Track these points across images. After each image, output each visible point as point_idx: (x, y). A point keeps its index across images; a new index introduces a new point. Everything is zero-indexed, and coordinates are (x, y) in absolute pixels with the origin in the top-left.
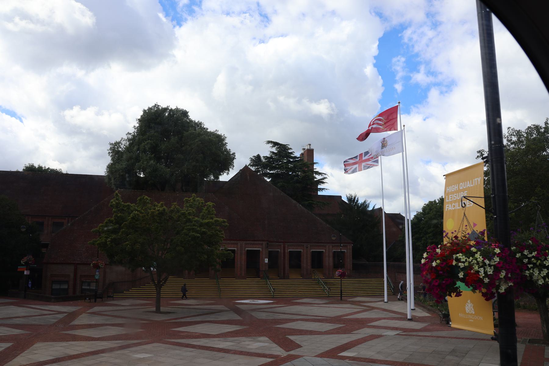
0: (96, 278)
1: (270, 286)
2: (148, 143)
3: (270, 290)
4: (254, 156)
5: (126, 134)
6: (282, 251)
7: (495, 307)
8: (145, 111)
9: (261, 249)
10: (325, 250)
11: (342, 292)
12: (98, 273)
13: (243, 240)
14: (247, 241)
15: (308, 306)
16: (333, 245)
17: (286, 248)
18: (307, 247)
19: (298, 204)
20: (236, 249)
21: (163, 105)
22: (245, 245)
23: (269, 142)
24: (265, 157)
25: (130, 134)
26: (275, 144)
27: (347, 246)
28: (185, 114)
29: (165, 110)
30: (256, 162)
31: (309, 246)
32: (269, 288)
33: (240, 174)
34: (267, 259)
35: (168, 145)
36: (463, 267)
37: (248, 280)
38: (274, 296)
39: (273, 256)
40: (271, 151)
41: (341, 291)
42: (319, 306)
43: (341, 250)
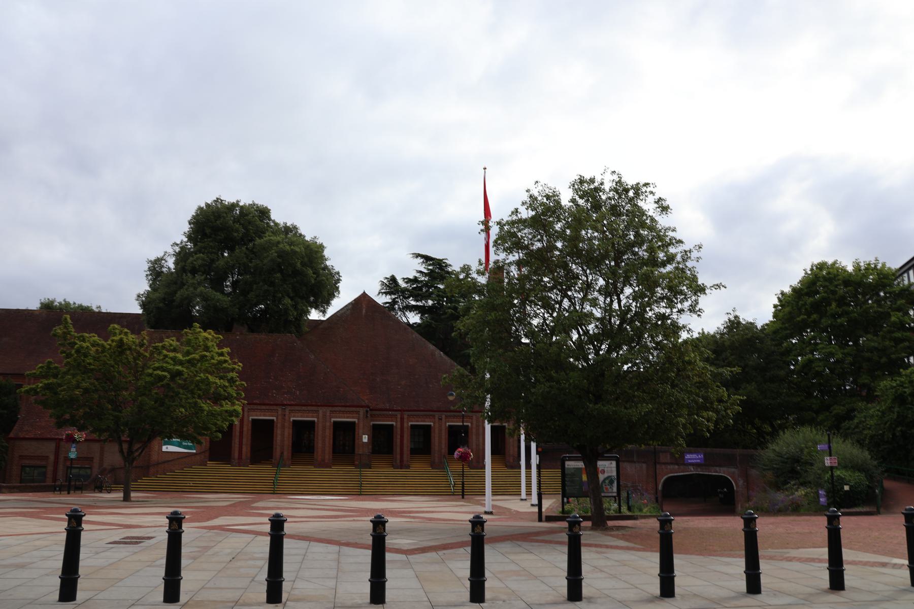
0: (71, 457)
1: (450, 479)
2: (197, 259)
3: (450, 484)
4: (386, 278)
5: (172, 246)
6: (399, 426)
9: (356, 420)
10: (472, 424)
11: (465, 491)
12: (75, 449)
13: (326, 406)
14: (333, 406)
17: (405, 420)
18: (441, 419)
19: (438, 351)
20: (432, 424)
21: (229, 199)
22: (330, 413)
23: (418, 256)
24: (406, 279)
25: (177, 245)
26: (427, 258)
27: (397, 415)
28: (264, 213)
29: (233, 206)
30: (391, 288)
31: (444, 416)
32: (449, 482)
33: (350, 306)
34: (367, 436)
35: (229, 260)
36: (539, 457)
37: (335, 468)
38: (362, 493)
39: (377, 431)
40: (417, 271)
41: (463, 482)
43: (463, 423)
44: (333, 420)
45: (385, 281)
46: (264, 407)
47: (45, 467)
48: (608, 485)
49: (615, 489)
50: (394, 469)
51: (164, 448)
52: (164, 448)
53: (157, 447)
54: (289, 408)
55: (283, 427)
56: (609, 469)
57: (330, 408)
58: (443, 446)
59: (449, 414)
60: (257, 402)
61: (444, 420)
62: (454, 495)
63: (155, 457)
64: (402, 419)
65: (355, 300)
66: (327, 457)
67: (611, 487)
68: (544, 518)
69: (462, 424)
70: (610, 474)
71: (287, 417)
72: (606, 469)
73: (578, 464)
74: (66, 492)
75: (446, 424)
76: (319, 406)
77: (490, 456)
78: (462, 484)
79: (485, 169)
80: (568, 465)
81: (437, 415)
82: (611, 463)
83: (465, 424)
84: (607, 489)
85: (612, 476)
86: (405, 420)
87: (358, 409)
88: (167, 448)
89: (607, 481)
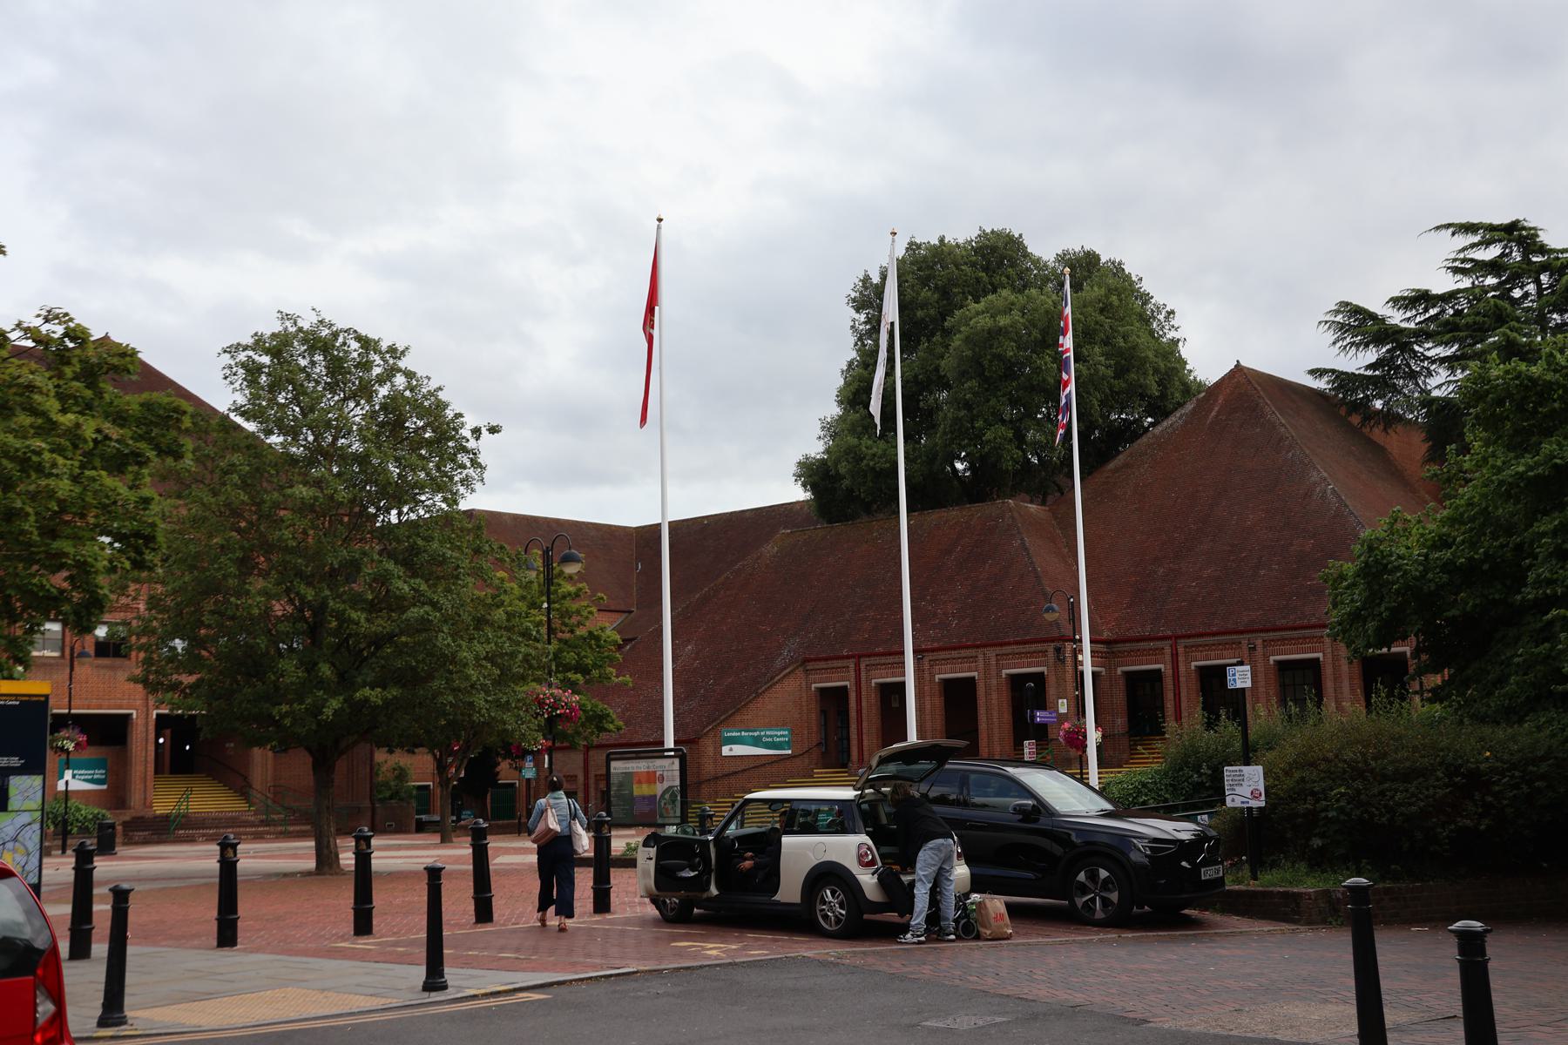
6: (1170, 672)
12: (532, 764)
14: (1001, 645)
18: (1254, 648)
26: (1391, 299)
31: (1259, 642)
34: (1065, 701)
43: (70, 709)
44: (1005, 672)
45: (1339, 318)
49: (678, 814)
51: (726, 751)
52: (726, 751)
56: (670, 773)
57: (998, 650)
60: (881, 649)
61: (1260, 649)
63: (709, 768)
64: (1175, 656)
69: (67, 711)
70: (670, 784)
71: (927, 675)
72: (665, 773)
73: (627, 765)
74: (60, 852)
75: (999, 675)
76: (978, 647)
79: (660, 220)
80: (615, 769)
81: (1244, 639)
82: (673, 763)
83: (73, 711)
86: (1181, 659)
87: (1159, 644)
88: (731, 750)
89: (667, 796)
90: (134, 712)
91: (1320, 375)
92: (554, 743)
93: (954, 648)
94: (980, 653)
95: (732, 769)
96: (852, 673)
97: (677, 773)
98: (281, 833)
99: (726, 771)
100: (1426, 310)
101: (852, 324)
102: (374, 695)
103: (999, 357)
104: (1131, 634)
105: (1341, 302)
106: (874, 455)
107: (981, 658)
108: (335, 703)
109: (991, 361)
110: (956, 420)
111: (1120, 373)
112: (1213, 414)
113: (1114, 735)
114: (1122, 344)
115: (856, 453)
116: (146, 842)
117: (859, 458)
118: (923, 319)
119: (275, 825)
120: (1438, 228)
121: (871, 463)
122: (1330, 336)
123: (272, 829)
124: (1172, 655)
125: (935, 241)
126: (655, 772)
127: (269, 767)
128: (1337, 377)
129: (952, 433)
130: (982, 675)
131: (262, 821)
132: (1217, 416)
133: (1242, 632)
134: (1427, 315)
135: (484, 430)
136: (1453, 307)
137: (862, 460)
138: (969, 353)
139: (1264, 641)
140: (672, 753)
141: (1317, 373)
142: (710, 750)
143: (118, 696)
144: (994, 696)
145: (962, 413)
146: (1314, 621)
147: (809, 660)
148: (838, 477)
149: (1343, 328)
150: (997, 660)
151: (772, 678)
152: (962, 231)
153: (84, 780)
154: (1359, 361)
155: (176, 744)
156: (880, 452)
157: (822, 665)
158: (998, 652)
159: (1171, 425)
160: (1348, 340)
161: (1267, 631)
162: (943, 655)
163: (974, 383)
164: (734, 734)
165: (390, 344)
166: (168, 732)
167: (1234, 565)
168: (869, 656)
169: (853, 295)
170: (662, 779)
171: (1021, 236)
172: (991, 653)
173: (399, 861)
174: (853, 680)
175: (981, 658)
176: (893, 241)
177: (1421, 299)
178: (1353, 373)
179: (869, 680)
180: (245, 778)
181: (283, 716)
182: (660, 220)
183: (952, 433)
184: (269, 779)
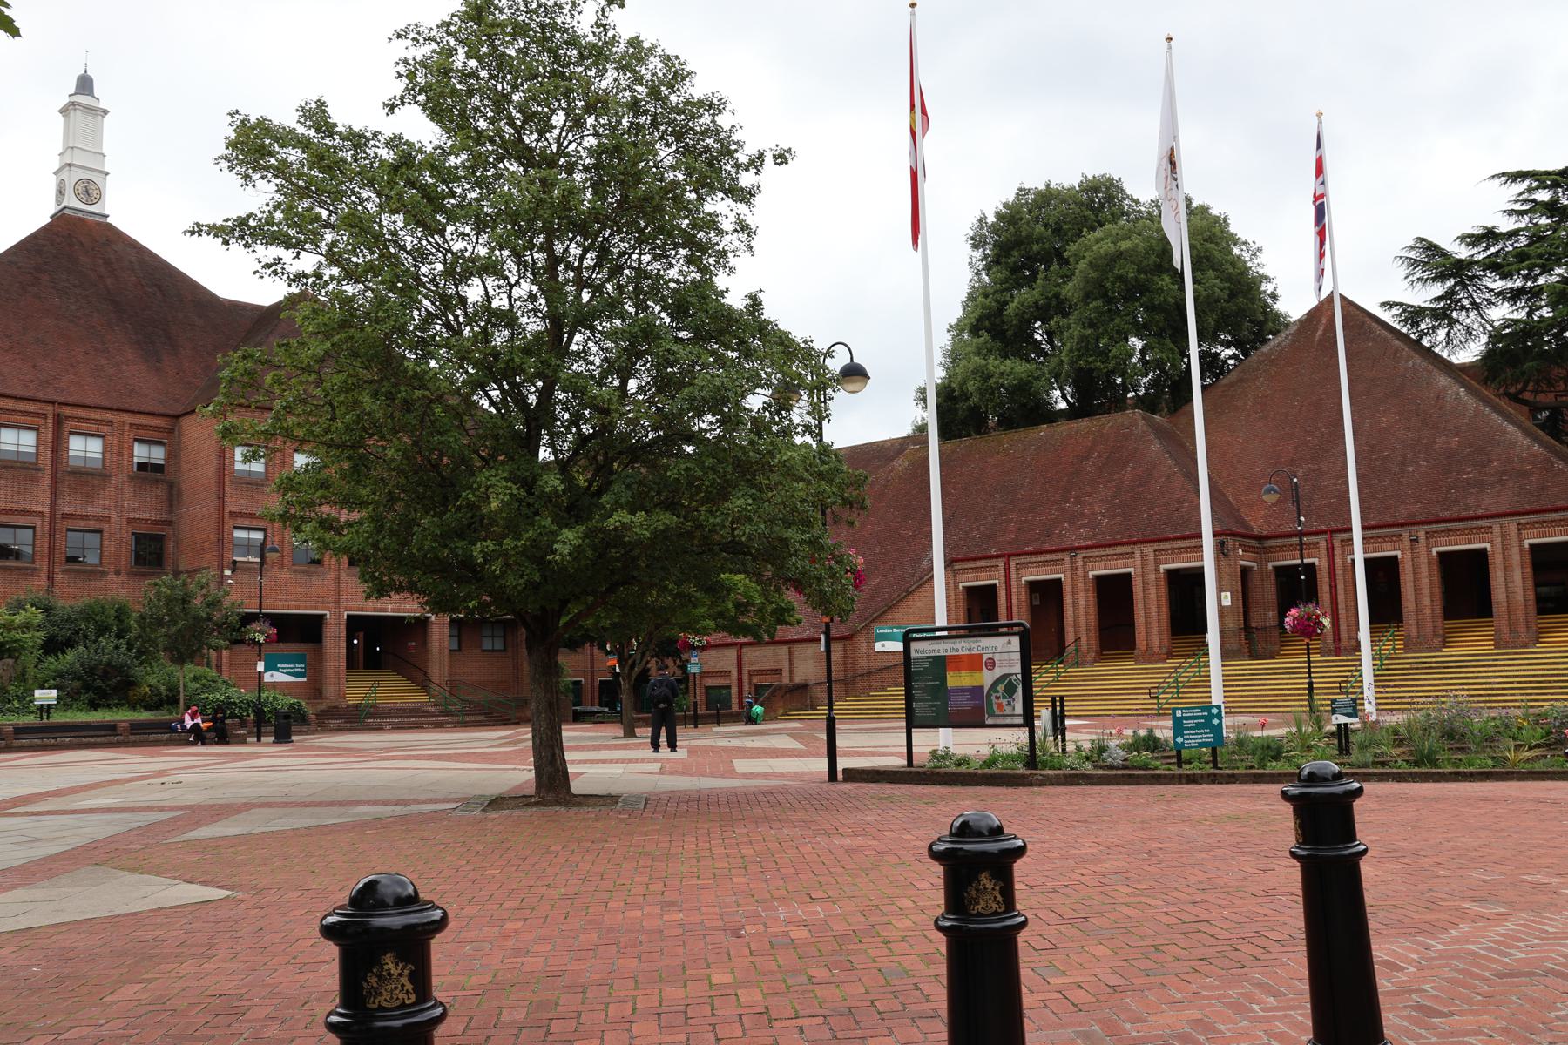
7: (995, 707)
8: (1022, 192)
14: (1160, 541)
15: (431, 801)
16: (1524, 520)
18: (1417, 541)
26: (1458, 238)
31: (1422, 534)
34: (1229, 594)
41: (1310, 684)
42: (33, 814)
44: (1163, 567)
45: (1412, 254)
46: (1041, 558)
47: (729, 687)
48: (1004, 697)
49: (1019, 709)
50: (1322, 656)
51: (878, 647)
52: (878, 647)
53: (864, 645)
54: (1083, 554)
55: (1074, 592)
56: (1005, 656)
57: (1156, 546)
58: (1427, 601)
59: (1434, 527)
60: (1031, 549)
61: (1422, 541)
62: (1160, 715)
65: (1307, 314)
66: (1156, 641)
67: (1009, 703)
68: (840, 776)
70: (1007, 671)
71: (1080, 573)
72: (997, 658)
75: (1157, 571)
76: (1134, 543)
77: (1368, 626)
78: (1308, 689)
79: (913, 5)
80: (917, 652)
81: (1405, 532)
84: (1000, 706)
85: (1012, 674)
86: (1337, 552)
88: (883, 646)
89: (1001, 688)
90: (328, 613)
91: (1391, 307)
92: (1301, 540)
93: (1110, 546)
94: (1137, 550)
95: (885, 664)
96: (1002, 572)
97: (1018, 656)
98: (458, 722)
99: (879, 665)
100: (1487, 248)
101: (969, 260)
102: (639, 524)
103: (1120, 278)
104: (1283, 529)
105: (1418, 238)
106: (1003, 373)
107: (1138, 553)
108: (570, 537)
109: (1113, 283)
110: (1082, 338)
111: (1232, 295)
112: (1320, 332)
113: (1266, 628)
114: (1231, 270)
115: (983, 373)
116: (340, 730)
117: (987, 377)
118: (1039, 252)
119: (452, 715)
120: (1493, 177)
121: (1001, 381)
122: (1404, 271)
123: (450, 719)
124: (1328, 549)
125: (1042, 187)
126: (981, 655)
127: (446, 664)
128: (1404, 311)
129: (1078, 350)
130: (1139, 571)
131: (441, 712)
132: (1324, 334)
133: (1402, 525)
134: (1489, 253)
135: (769, 160)
136: (1512, 245)
137: (989, 378)
138: (1095, 275)
139: (1427, 533)
140: (945, 633)
141: (1389, 305)
142: (864, 646)
143: (314, 598)
144: (1153, 592)
145: (1089, 331)
146: (1480, 512)
147: (957, 561)
148: (965, 396)
149: (1415, 263)
150: (1156, 556)
151: (921, 578)
152: (1068, 177)
153: (287, 673)
154: (1426, 295)
155: (369, 644)
156: (1008, 370)
157: (971, 565)
158: (1157, 548)
159: (1279, 344)
160: (1418, 275)
161: (1430, 523)
162: (1096, 552)
163: (1099, 303)
164: (886, 631)
165: (634, 35)
166: (361, 635)
167: (1378, 464)
168: (1019, 555)
169: (972, 233)
170: (991, 664)
171: (1120, 179)
172: (1149, 549)
173: (619, 768)
174: (1003, 579)
175: (1138, 553)
176: (1170, 48)
177: (1490, 235)
178: (1419, 307)
179: (1019, 578)
180: (425, 673)
181: (488, 558)
182: (913, 5)
183: (1078, 350)
184: (446, 674)
